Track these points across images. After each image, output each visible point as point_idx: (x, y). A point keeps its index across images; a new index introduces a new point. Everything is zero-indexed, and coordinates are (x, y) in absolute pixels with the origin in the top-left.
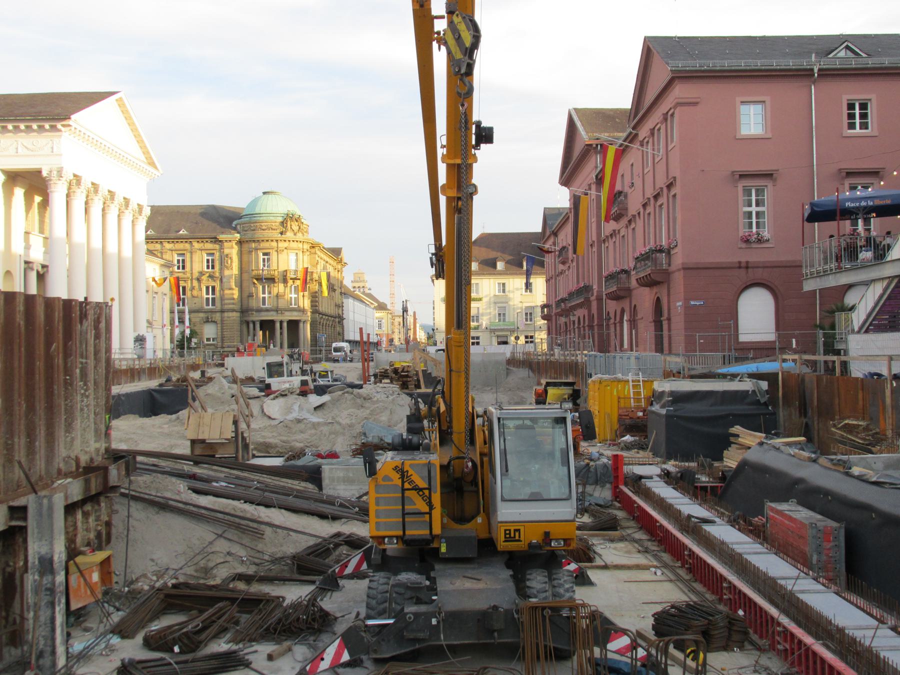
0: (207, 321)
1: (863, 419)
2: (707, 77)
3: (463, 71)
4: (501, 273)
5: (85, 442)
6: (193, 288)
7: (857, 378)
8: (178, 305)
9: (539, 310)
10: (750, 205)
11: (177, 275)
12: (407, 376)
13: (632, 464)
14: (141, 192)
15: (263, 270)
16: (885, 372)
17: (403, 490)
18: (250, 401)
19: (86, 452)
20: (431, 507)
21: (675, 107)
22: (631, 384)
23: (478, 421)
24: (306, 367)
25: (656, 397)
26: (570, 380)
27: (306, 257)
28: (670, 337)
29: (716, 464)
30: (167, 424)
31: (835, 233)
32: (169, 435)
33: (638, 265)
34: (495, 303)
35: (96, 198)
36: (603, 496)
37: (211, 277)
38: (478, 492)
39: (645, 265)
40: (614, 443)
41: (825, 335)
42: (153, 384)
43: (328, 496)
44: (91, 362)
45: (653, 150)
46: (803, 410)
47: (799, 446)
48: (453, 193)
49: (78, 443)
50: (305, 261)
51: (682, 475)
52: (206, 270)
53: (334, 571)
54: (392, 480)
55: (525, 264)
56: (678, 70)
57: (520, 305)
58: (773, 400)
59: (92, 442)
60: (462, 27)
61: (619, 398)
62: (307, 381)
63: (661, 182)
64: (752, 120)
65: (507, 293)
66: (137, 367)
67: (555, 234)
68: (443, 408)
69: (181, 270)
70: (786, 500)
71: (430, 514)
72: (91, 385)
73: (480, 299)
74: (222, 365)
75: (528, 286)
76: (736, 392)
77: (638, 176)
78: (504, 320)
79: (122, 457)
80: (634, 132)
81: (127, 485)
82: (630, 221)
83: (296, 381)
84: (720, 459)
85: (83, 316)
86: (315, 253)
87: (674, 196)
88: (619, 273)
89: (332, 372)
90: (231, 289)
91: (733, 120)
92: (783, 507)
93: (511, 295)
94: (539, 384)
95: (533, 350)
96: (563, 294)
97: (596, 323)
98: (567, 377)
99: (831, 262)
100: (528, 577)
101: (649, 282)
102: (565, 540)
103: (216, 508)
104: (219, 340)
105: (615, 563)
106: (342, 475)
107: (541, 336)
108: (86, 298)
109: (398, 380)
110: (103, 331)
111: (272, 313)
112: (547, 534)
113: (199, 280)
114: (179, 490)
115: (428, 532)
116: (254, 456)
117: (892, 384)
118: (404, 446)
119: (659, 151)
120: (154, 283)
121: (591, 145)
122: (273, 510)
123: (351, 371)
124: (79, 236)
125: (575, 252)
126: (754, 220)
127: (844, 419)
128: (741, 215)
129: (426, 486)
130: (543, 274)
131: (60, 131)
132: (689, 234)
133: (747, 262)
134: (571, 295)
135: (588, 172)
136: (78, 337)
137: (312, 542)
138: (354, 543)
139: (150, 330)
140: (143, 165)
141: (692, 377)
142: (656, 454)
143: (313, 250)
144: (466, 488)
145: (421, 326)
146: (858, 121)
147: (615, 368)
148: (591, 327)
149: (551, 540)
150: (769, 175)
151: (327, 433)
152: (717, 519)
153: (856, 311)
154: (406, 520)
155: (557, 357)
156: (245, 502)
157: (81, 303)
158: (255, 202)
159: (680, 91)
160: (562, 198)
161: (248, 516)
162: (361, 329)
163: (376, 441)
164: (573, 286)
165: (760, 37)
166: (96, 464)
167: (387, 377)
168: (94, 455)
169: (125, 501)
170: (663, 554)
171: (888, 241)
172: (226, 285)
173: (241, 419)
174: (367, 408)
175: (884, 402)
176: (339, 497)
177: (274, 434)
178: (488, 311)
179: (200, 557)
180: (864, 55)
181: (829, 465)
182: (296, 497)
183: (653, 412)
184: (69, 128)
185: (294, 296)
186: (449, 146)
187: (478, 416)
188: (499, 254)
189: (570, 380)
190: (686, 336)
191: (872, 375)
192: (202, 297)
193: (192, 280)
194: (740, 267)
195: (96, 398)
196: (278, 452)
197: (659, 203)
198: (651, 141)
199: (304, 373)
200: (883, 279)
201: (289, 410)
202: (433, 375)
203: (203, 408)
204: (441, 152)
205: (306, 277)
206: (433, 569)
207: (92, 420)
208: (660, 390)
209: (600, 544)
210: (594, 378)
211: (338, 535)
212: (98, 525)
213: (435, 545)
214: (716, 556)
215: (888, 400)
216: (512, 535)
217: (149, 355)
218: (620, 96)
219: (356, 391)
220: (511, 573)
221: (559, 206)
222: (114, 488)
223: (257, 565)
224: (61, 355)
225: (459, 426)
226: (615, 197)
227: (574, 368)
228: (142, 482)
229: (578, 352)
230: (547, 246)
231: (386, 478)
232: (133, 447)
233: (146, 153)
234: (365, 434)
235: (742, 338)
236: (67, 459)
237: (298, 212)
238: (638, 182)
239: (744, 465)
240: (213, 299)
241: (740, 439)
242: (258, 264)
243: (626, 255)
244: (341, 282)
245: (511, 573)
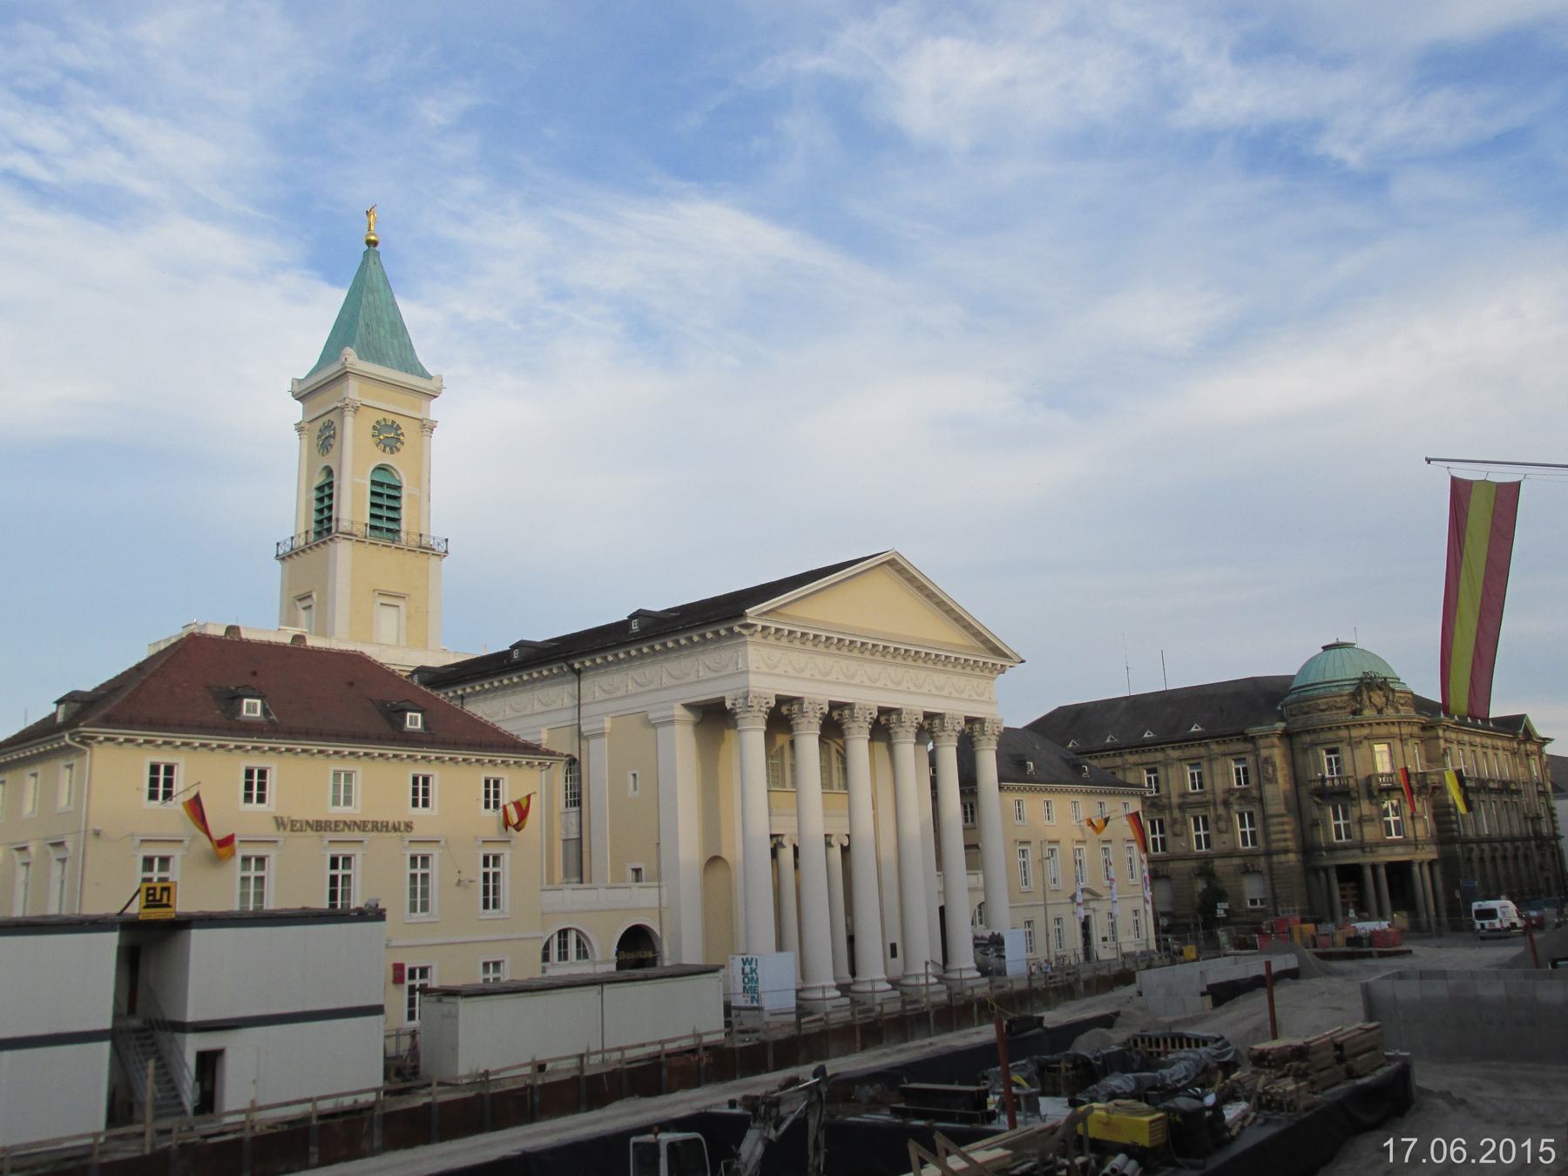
0: (1246, 871)
86: (1438, 738)
113: (1226, 804)
131: (740, 635)
242: (1323, 767)
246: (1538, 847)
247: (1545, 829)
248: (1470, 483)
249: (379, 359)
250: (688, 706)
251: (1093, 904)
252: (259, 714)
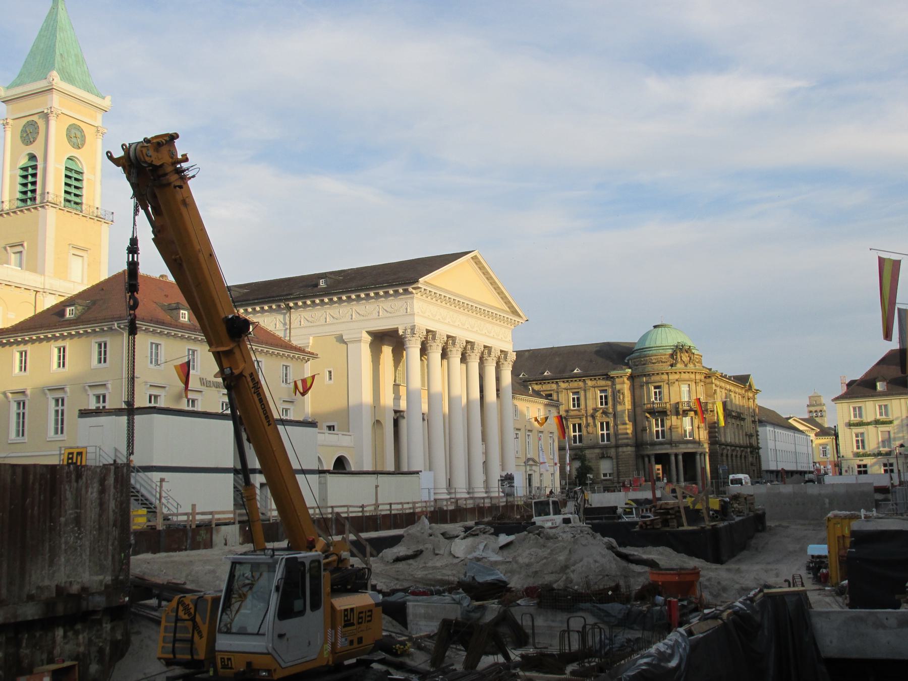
0: (603, 457)
6: (588, 425)
14: (504, 339)
37: (605, 413)
73: (891, 422)
86: (712, 383)
90: (625, 424)
104: (615, 475)
108: (115, 461)
112: (249, 664)
113: (593, 417)
124: (438, 385)
143: (708, 380)
154: (176, 645)
158: (644, 338)
177: (454, 572)
178: (901, 435)
193: (586, 417)
201: (474, 548)
237: (688, 343)
240: (608, 435)
246: (751, 452)
247: (755, 444)
248: (884, 259)
249: (69, 79)
250: (369, 333)
251: (534, 468)
252: (187, 319)
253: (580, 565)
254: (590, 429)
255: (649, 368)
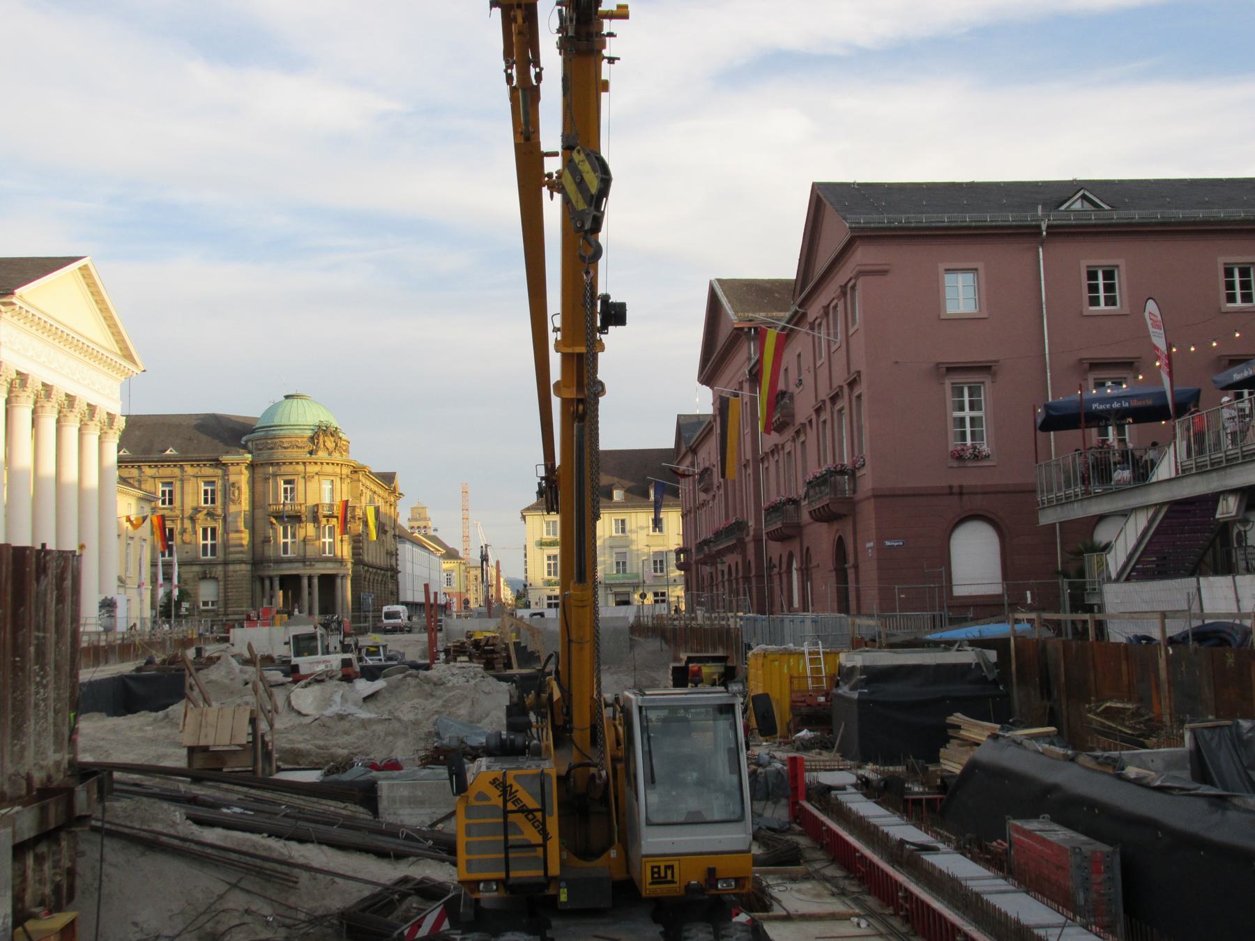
0: (204, 577)
1: (1130, 700)
2: (977, 235)
3: (587, 226)
4: (618, 506)
5: (40, 752)
6: (184, 531)
7: (1118, 645)
8: (163, 555)
9: (673, 557)
10: (962, 409)
11: (161, 513)
12: (492, 651)
13: (816, 770)
14: (109, 396)
15: (284, 504)
16: (1156, 634)
17: (506, 813)
18: (274, 690)
19: (42, 768)
20: (545, 836)
21: (857, 277)
22: (807, 657)
23: (607, 713)
24: (348, 640)
25: (845, 674)
26: (720, 653)
27: (345, 487)
28: (858, 590)
29: (932, 768)
30: (148, 725)
31: (1081, 448)
32: (153, 741)
33: (811, 492)
34: (611, 547)
35: (48, 406)
36: (776, 816)
37: (211, 514)
38: (610, 814)
39: (821, 492)
40: (787, 742)
41: (1071, 585)
42: (127, 668)
43: (388, 824)
44: (52, 636)
45: (828, 335)
46: (1046, 689)
47: (1048, 740)
48: (572, 394)
49: (30, 755)
50: (344, 492)
51: (886, 784)
52: (202, 504)
53: (402, 933)
54: (488, 799)
55: (652, 492)
56: (858, 226)
57: (646, 550)
58: (1004, 677)
59: (50, 752)
60: (586, 168)
61: (791, 677)
62: (350, 660)
63: (840, 378)
64: (961, 294)
65: (628, 534)
66: (103, 643)
67: (694, 451)
68: (557, 695)
69: (167, 506)
70: (1036, 816)
71: (544, 846)
72: (50, 669)
74: (226, 640)
75: (657, 523)
76: (955, 666)
77: (808, 369)
78: (624, 571)
79: (95, 773)
80: (801, 311)
81: (99, 815)
82: (798, 433)
83: (335, 660)
84: (936, 760)
85: (42, 570)
87: (859, 397)
88: (784, 504)
89: (385, 647)
91: (936, 294)
92: (1032, 825)
93: (634, 536)
94: (677, 659)
95: (665, 612)
96: (706, 534)
97: (753, 573)
98: (715, 649)
99: (1076, 485)
100: (686, 934)
101: (826, 516)
102: (737, 880)
103: (229, 845)
104: (221, 604)
105: (801, 911)
106: (406, 793)
107: (677, 593)
109: (479, 658)
110: (69, 591)
111: (296, 565)
112: (711, 872)
113: (192, 519)
114: (174, 820)
115: (541, 873)
116: (279, 769)
117: (1167, 651)
118: (501, 750)
119: (836, 335)
120: (128, 524)
121: (742, 329)
122: (310, 846)
123: (411, 646)
125: (723, 476)
126: (968, 429)
127: (1101, 700)
128: (950, 423)
129: (538, 806)
130: (677, 506)
132: (874, 448)
133: (961, 487)
134: (718, 535)
135: (739, 367)
136: (33, 600)
137: (367, 891)
138: (429, 891)
139: (122, 590)
140: (119, 361)
141: (892, 646)
142: (845, 755)
143: (355, 476)
144: (594, 809)
145: (505, 581)
146: (1102, 294)
147: (783, 637)
148: (747, 579)
149: (717, 880)
150: (986, 368)
151: (382, 734)
152: (941, 846)
153: (1113, 552)
154: (511, 855)
155: (700, 621)
156: (270, 836)
157: (39, 552)
159: (863, 256)
160: (702, 402)
161: (275, 855)
162: (426, 586)
163: (455, 744)
164: (720, 523)
165: (967, 184)
166: (55, 784)
167: (463, 653)
168: (52, 771)
169: (98, 838)
170: (867, 898)
171: (1151, 454)
172: (231, 527)
173: (262, 716)
174: (439, 698)
175: (1157, 676)
176: (403, 826)
177: (306, 737)
179: (207, 917)
180: (1106, 207)
181: (1092, 764)
182: (342, 826)
183: (840, 697)
184: (11, 307)
185: (328, 540)
186: (565, 329)
187: (607, 705)
188: (616, 479)
189: (720, 653)
190: (880, 589)
191: (1139, 639)
192: (197, 544)
193: (182, 519)
194: (951, 494)
195: (57, 688)
196: (312, 762)
197: (837, 407)
198: (824, 323)
199: (345, 648)
200: (1147, 507)
201: (328, 702)
202: (530, 649)
203: (206, 700)
204: (553, 337)
205: (346, 514)
206: (549, 927)
207: (51, 720)
208: (849, 664)
209: (778, 885)
210: (756, 650)
211: (405, 880)
212: (55, 874)
213: (551, 891)
214: (943, 898)
215: (1163, 674)
216: (663, 874)
217: (121, 626)
218: (780, 261)
219: (422, 673)
220: (662, 929)
221: (698, 412)
222: (83, 819)
223: (288, 927)
224: (9, 627)
225: (582, 718)
226: (778, 399)
227: (725, 637)
228: (120, 807)
229: (730, 614)
230: (682, 468)
231: (481, 796)
232: (103, 759)
233: (120, 341)
234: (438, 734)
235: (958, 591)
236: (13, 778)
238: (808, 379)
239: (972, 768)
240: (213, 546)
241: (962, 732)
243: (793, 479)
244: (395, 521)
245: (662, 929)
253: (487, 721)
254: (187, 537)
255: (279, 454)
